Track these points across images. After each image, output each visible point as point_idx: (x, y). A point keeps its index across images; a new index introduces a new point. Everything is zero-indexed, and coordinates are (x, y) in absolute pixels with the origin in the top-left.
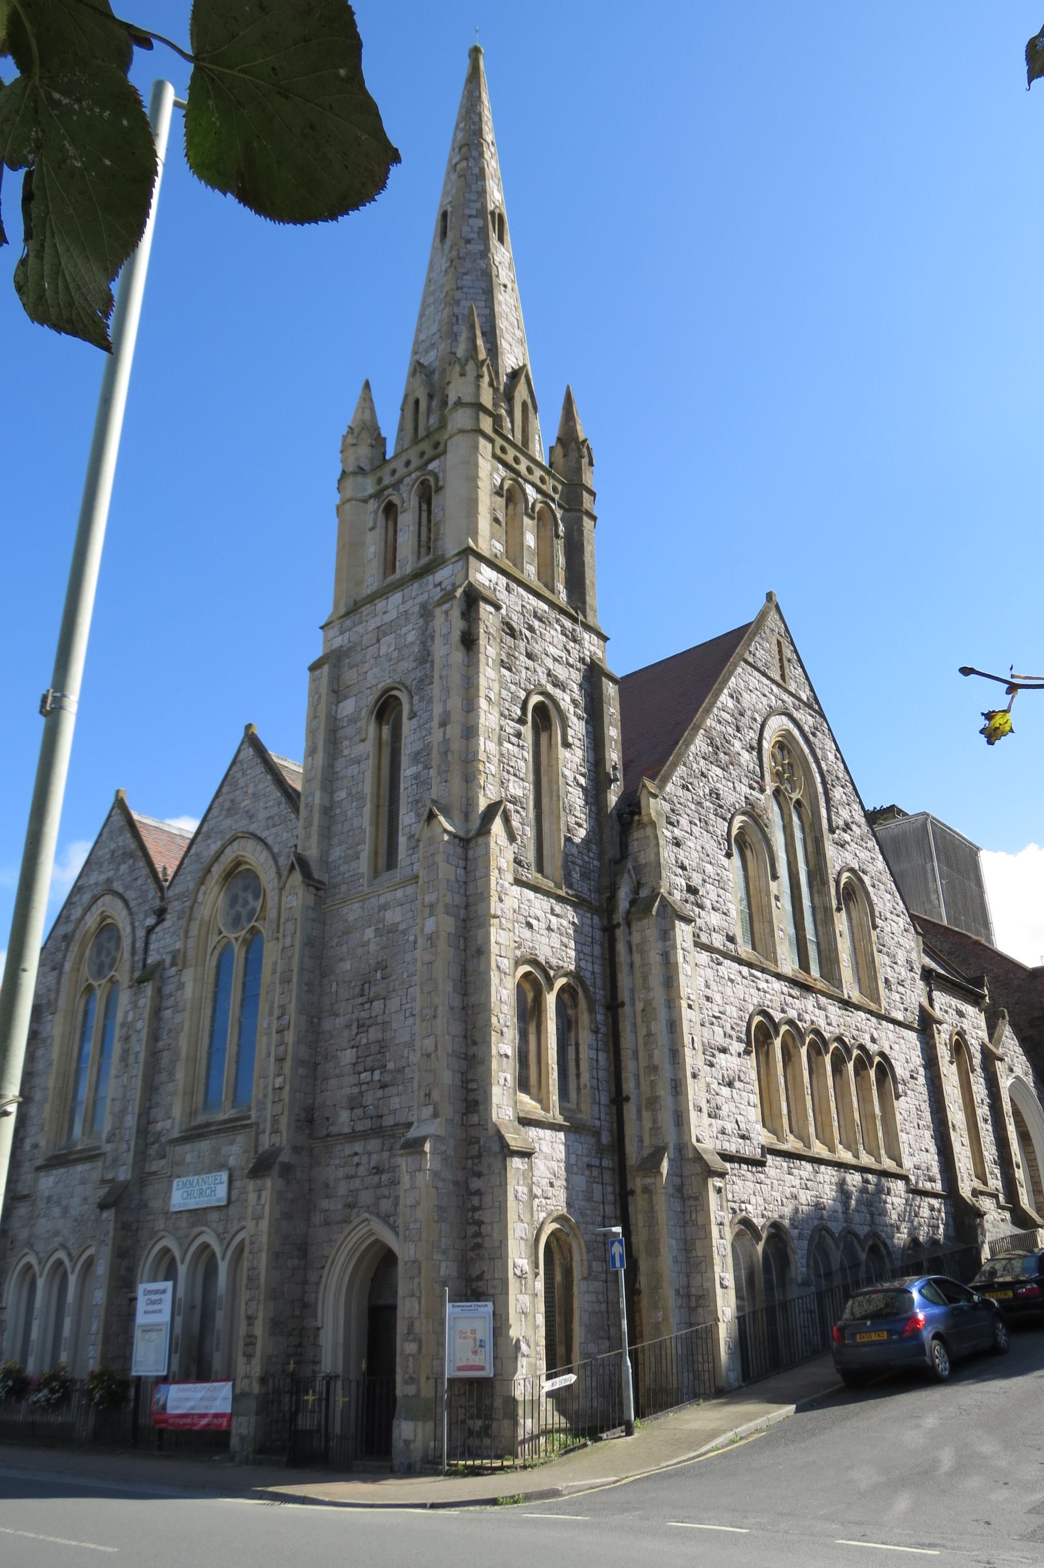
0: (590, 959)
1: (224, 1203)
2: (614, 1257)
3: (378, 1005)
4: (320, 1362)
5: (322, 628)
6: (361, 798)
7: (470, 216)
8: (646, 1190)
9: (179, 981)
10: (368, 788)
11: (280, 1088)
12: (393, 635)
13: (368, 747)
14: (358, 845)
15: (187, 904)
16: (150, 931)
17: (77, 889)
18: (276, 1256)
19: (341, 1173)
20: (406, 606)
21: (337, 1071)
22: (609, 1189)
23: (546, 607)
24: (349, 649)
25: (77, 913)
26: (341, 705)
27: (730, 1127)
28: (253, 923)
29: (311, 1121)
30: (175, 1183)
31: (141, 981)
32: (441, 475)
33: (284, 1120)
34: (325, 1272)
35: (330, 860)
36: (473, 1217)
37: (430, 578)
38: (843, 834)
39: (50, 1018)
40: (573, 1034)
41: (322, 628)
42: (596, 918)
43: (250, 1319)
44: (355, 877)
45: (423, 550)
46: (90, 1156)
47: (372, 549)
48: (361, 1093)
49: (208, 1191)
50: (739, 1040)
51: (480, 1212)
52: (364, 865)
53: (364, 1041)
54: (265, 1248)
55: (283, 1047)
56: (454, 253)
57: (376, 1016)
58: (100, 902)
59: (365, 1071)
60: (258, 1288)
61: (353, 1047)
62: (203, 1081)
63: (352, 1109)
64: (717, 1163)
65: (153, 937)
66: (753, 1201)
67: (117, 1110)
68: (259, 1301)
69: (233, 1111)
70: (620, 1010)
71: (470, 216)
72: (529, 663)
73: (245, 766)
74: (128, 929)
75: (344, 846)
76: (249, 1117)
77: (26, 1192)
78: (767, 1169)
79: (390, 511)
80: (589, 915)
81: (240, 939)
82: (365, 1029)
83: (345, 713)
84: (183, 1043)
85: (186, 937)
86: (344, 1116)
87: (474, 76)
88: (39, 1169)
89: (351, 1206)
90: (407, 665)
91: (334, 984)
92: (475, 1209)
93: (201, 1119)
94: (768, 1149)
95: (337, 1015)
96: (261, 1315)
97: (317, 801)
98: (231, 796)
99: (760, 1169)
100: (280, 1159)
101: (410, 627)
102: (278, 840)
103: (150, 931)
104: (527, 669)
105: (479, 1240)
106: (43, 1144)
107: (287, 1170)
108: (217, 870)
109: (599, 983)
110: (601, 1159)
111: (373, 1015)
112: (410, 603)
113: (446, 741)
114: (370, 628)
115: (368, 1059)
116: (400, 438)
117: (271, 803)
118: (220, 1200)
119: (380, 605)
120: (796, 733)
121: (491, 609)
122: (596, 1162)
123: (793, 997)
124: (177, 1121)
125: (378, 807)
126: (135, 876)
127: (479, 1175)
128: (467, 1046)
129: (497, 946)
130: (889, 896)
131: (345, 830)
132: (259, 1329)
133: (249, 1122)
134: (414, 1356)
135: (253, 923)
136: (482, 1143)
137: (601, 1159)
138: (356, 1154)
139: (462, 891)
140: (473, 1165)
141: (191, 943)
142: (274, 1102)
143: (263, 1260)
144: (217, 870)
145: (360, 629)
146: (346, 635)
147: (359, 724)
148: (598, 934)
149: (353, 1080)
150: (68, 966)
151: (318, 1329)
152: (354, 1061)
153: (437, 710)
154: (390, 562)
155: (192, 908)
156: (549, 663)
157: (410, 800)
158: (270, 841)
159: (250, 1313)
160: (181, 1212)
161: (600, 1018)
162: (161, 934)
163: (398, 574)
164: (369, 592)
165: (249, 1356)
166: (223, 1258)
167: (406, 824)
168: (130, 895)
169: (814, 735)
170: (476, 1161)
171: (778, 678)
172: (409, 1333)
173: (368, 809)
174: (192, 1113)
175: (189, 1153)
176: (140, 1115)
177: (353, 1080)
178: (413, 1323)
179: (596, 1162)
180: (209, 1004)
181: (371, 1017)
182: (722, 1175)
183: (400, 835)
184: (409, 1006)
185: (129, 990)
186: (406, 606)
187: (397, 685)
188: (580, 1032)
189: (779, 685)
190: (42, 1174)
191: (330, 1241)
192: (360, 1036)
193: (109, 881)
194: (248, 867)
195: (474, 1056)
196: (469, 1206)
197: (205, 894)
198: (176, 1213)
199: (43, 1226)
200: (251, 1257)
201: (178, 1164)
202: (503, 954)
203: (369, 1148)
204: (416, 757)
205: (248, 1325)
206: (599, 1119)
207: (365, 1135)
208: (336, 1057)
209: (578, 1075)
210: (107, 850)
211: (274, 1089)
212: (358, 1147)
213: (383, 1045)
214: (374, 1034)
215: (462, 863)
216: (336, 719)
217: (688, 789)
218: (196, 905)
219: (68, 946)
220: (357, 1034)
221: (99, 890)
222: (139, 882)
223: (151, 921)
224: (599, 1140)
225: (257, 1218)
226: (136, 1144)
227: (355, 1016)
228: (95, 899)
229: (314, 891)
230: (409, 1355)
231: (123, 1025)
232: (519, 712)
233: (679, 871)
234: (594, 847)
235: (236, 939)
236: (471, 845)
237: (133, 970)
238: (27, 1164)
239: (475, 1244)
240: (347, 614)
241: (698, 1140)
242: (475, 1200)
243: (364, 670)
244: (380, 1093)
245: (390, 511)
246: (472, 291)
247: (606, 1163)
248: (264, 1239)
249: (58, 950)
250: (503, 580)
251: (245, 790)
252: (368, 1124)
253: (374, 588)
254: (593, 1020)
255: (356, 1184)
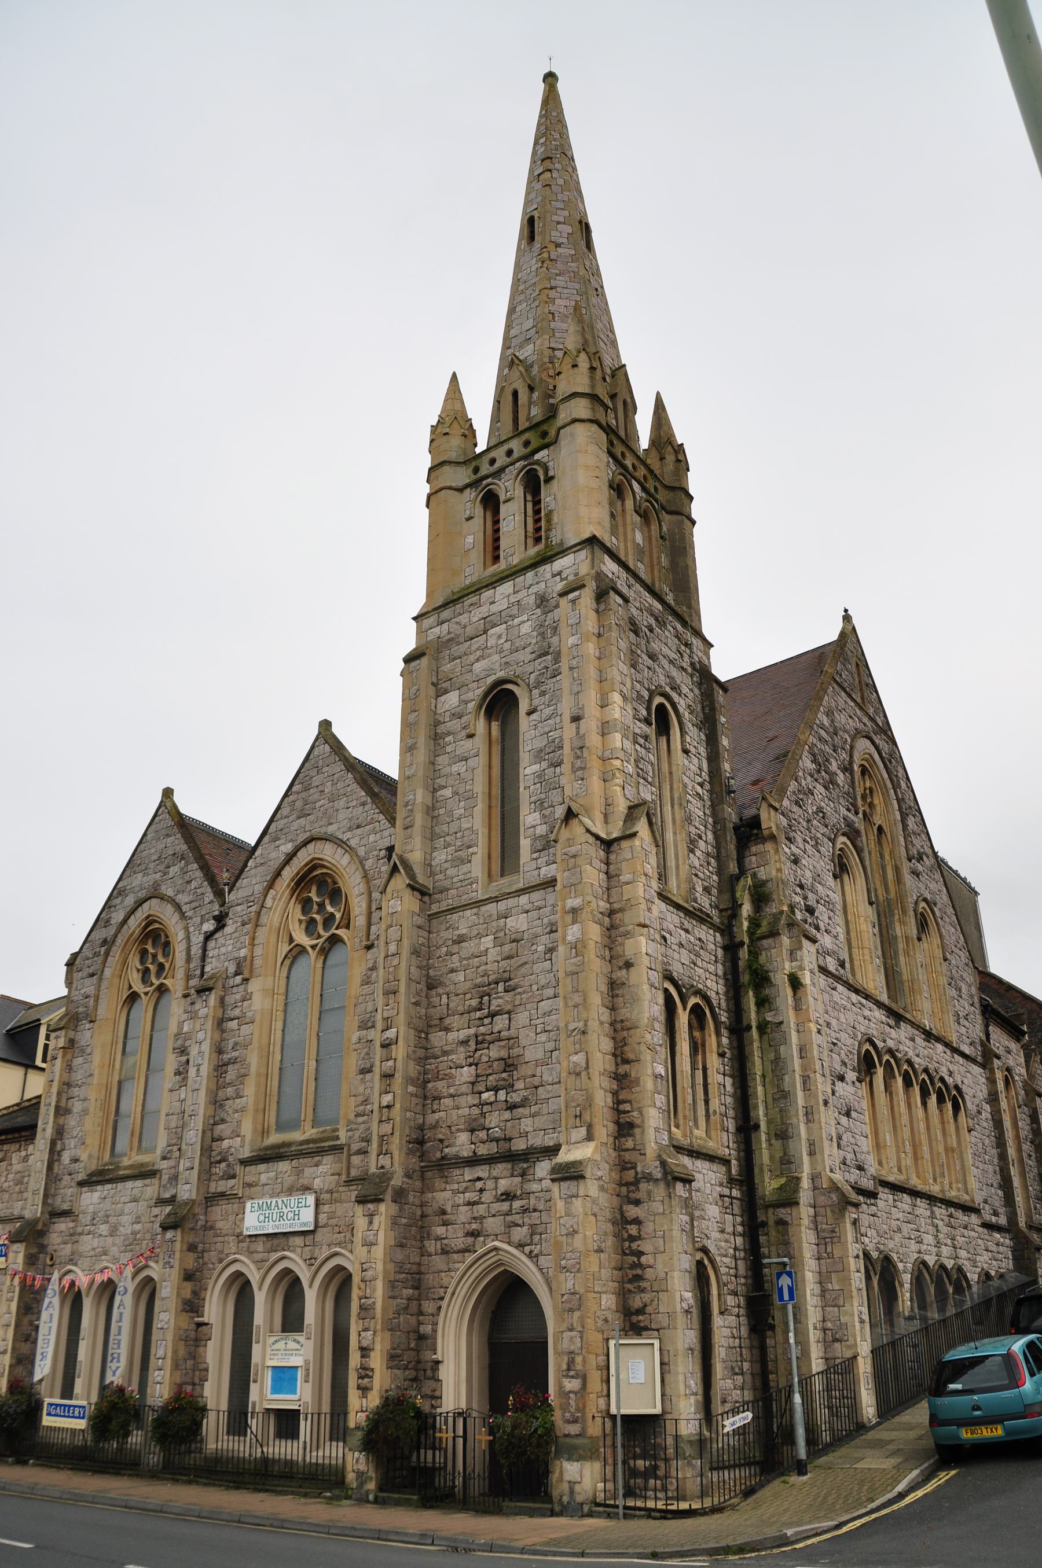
0: (714, 978)
1: (312, 1228)
2: (781, 1290)
3: (501, 1022)
4: (441, 1398)
5: (414, 619)
6: (471, 797)
7: (558, 223)
8: (782, 1223)
9: (245, 990)
10: (479, 787)
11: (388, 1107)
12: (504, 626)
13: (479, 743)
14: (469, 847)
15: (254, 909)
16: (209, 937)
17: (118, 892)
18: (392, 1285)
19: (460, 1199)
20: (519, 596)
21: (452, 1091)
22: (739, 1219)
23: (660, 607)
24: (450, 640)
25: (118, 916)
26: (442, 699)
27: (850, 1157)
28: (333, 931)
29: (421, 1142)
30: (248, 1205)
31: (201, 991)
32: (551, 464)
33: (396, 1140)
34: (444, 1304)
35: (433, 863)
36: (630, 1246)
37: (548, 567)
38: (917, 864)
39: (88, 1026)
40: (700, 1057)
41: (414, 619)
42: (718, 934)
43: (365, 1351)
44: (467, 882)
45: (530, 541)
46: (145, 1173)
47: (470, 539)
48: (483, 1114)
49: (291, 1215)
50: (853, 1070)
51: (639, 1242)
52: (477, 868)
53: (485, 1059)
54: (381, 1277)
55: (391, 1063)
56: (545, 255)
57: (500, 1032)
58: (146, 905)
59: (487, 1090)
60: (374, 1318)
61: (470, 1065)
62: (275, 1098)
63: (472, 1131)
64: (853, 1196)
65: (211, 944)
66: (869, 1235)
67: (173, 1125)
68: (375, 1332)
69: (315, 1131)
70: (746, 1035)
71: (558, 223)
72: (650, 662)
73: (320, 762)
74: (181, 935)
75: (451, 849)
76: (338, 1138)
77: (65, 1207)
78: (878, 1201)
79: (491, 502)
80: (711, 932)
81: (318, 948)
82: (486, 1045)
83: (447, 707)
84: (253, 1060)
85: (253, 945)
86: (463, 1138)
87: (551, 101)
88: (81, 1184)
89: (474, 1234)
90: (525, 656)
91: (444, 997)
92: (632, 1239)
93: (274, 1138)
94: (880, 1181)
95: (447, 1029)
96: (378, 1347)
97: (419, 799)
98: (304, 795)
99: (873, 1201)
100: (392, 1183)
101: (525, 618)
102: (364, 842)
103: (209, 937)
104: (649, 668)
105: (639, 1272)
106: (84, 1157)
107: (399, 1195)
108: (288, 873)
109: (724, 1005)
110: (731, 1189)
111: (495, 1030)
112: (524, 593)
113: (580, 736)
114: (475, 619)
115: (491, 1078)
116: (496, 417)
117: (354, 803)
118: (305, 1224)
119: (487, 594)
120: (876, 757)
121: (619, 600)
122: (727, 1192)
123: (891, 1027)
124: (248, 1139)
125: (490, 807)
126: (187, 878)
127: (637, 1203)
128: (617, 1065)
129: (648, 958)
130: (953, 930)
131: (452, 831)
132: (377, 1361)
133: (339, 1142)
134: (576, 1393)
135: (333, 931)
136: (639, 1169)
137: (731, 1189)
138: (479, 1179)
139: (605, 897)
140: (629, 1192)
141: (258, 951)
142: (381, 1121)
143: (379, 1292)
144: (288, 873)
145: (463, 619)
146: (445, 626)
147: (464, 719)
148: (720, 953)
149: (472, 1100)
150: (108, 972)
151: (438, 1362)
152: (472, 1079)
153: (566, 708)
154: (494, 550)
155: (258, 914)
156: (665, 662)
157: (532, 799)
158: (353, 843)
159: (365, 1344)
160: (256, 1236)
161: (725, 1041)
162: (221, 941)
163: (502, 565)
164: (467, 582)
165: (364, 1390)
166: (311, 1286)
167: (528, 825)
168: (182, 899)
169: (890, 762)
170: (633, 1188)
171: (859, 700)
172: (569, 1369)
173: (480, 809)
174: (265, 1133)
175: (264, 1173)
176: (204, 1132)
177: (472, 1100)
178: (573, 1359)
179: (727, 1192)
180: (280, 1015)
181: (492, 1033)
182: (857, 1205)
183: (522, 838)
184: (541, 1020)
185: (183, 1000)
186: (519, 596)
187: (515, 680)
188: (708, 1054)
189: (861, 708)
190: (85, 1189)
191: (449, 1270)
192: (479, 1053)
193: (156, 885)
194: (325, 871)
195: (626, 1076)
196: (625, 1235)
197: (274, 899)
198: (250, 1236)
199: (87, 1244)
200: (363, 1286)
201: (250, 1185)
202: (653, 967)
203: (495, 1173)
204: (539, 755)
205: (362, 1357)
206: (728, 1147)
207: (490, 1160)
208: (451, 1077)
209: (707, 1102)
210: (153, 851)
211: (381, 1108)
212: (481, 1171)
213: (510, 1061)
214: (495, 1052)
215: (604, 867)
216: (435, 713)
217: (800, 807)
218: (264, 910)
219: (107, 954)
220: (476, 1050)
221: (142, 894)
222: (194, 884)
223: (209, 926)
224: (729, 1171)
225: (369, 1244)
226: (200, 1163)
227: (472, 1031)
228: (140, 903)
229: (419, 897)
230: (570, 1392)
231: (177, 1035)
232: (645, 713)
233: (798, 890)
234: (713, 860)
235: (313, 947)
236: (612, 849)
237: (188, 977)
238: (67, 1178)
239: (634, 1276)
240: (445, 605)
241: (831, 1171)
242: (633, 1230)
243: (468, 662)
244: (507, 1115)
245: (491, 502)
246: (566, 291)
247: (735, 1193)
248: (380, 1267)
249: (96, 954)
250: (624, 574)
251: (321, 788)
252: (493, 1148)
253: (475, 579)
254: (719, 1044)
255: (481, 1209)
